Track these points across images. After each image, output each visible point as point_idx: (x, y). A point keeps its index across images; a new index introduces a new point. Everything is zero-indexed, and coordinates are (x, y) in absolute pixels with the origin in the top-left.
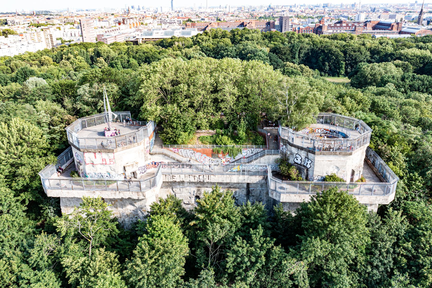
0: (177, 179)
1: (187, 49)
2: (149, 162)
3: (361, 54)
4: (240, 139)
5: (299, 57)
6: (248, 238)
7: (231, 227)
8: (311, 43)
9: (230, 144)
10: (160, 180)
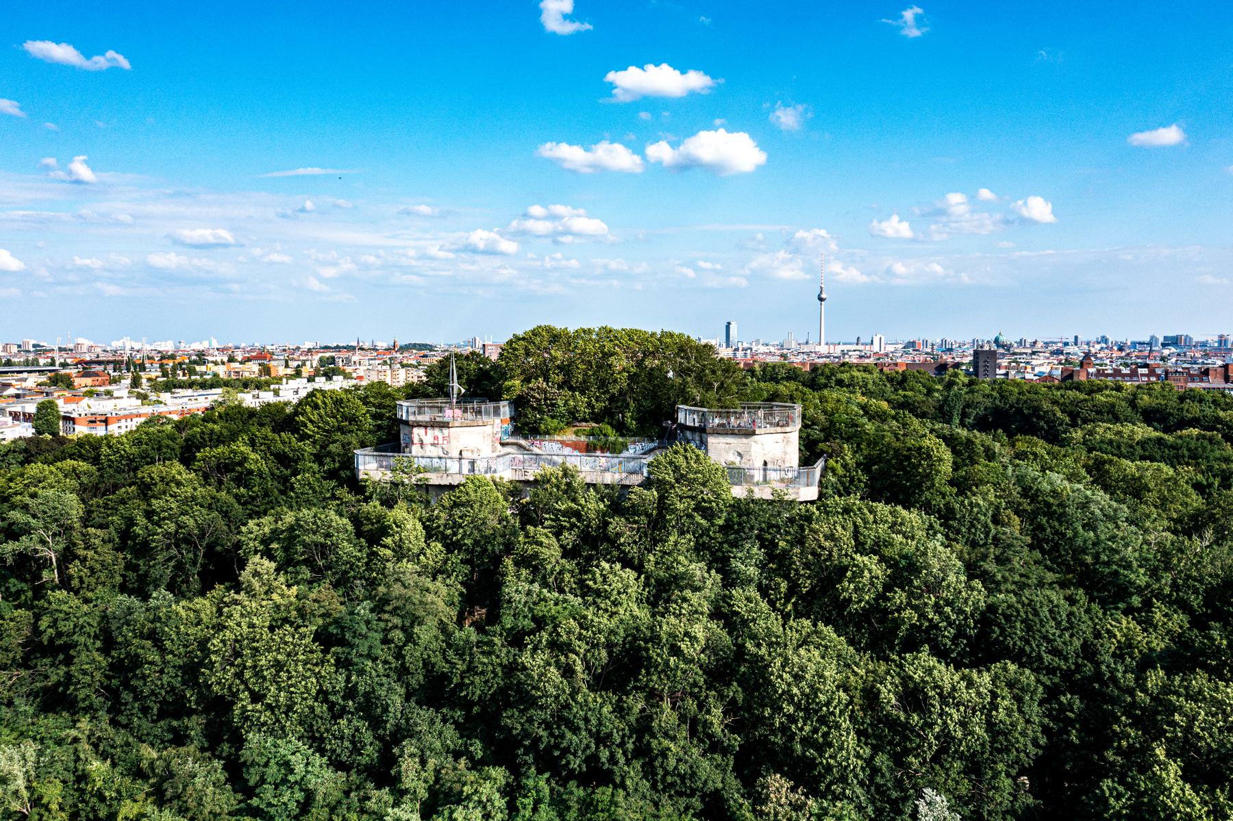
4: (628, 430)
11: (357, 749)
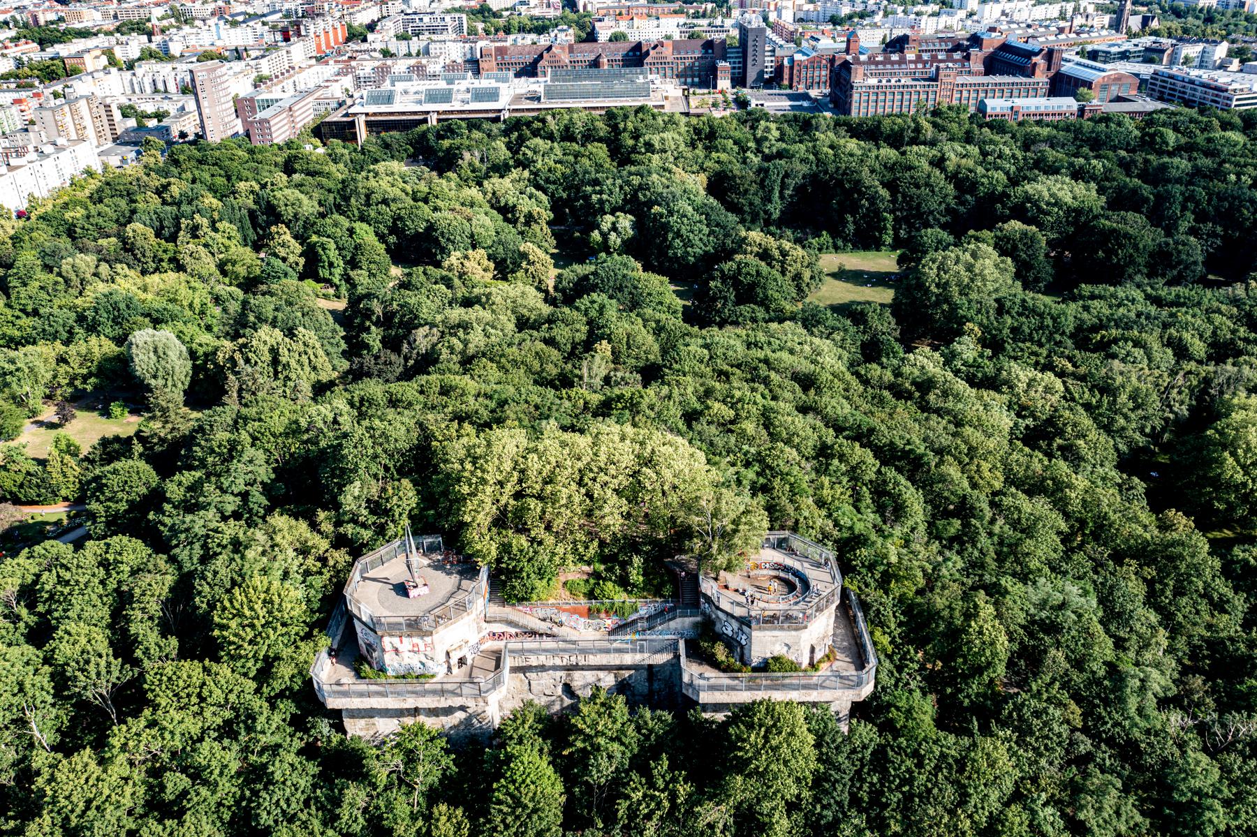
0: (534, 661)
1: (495, 180)
2: (485, 633)
3: (933, 191)
5: (782, 197)
6: (646, 772)
7: (623, 753)
8: (811, 157)
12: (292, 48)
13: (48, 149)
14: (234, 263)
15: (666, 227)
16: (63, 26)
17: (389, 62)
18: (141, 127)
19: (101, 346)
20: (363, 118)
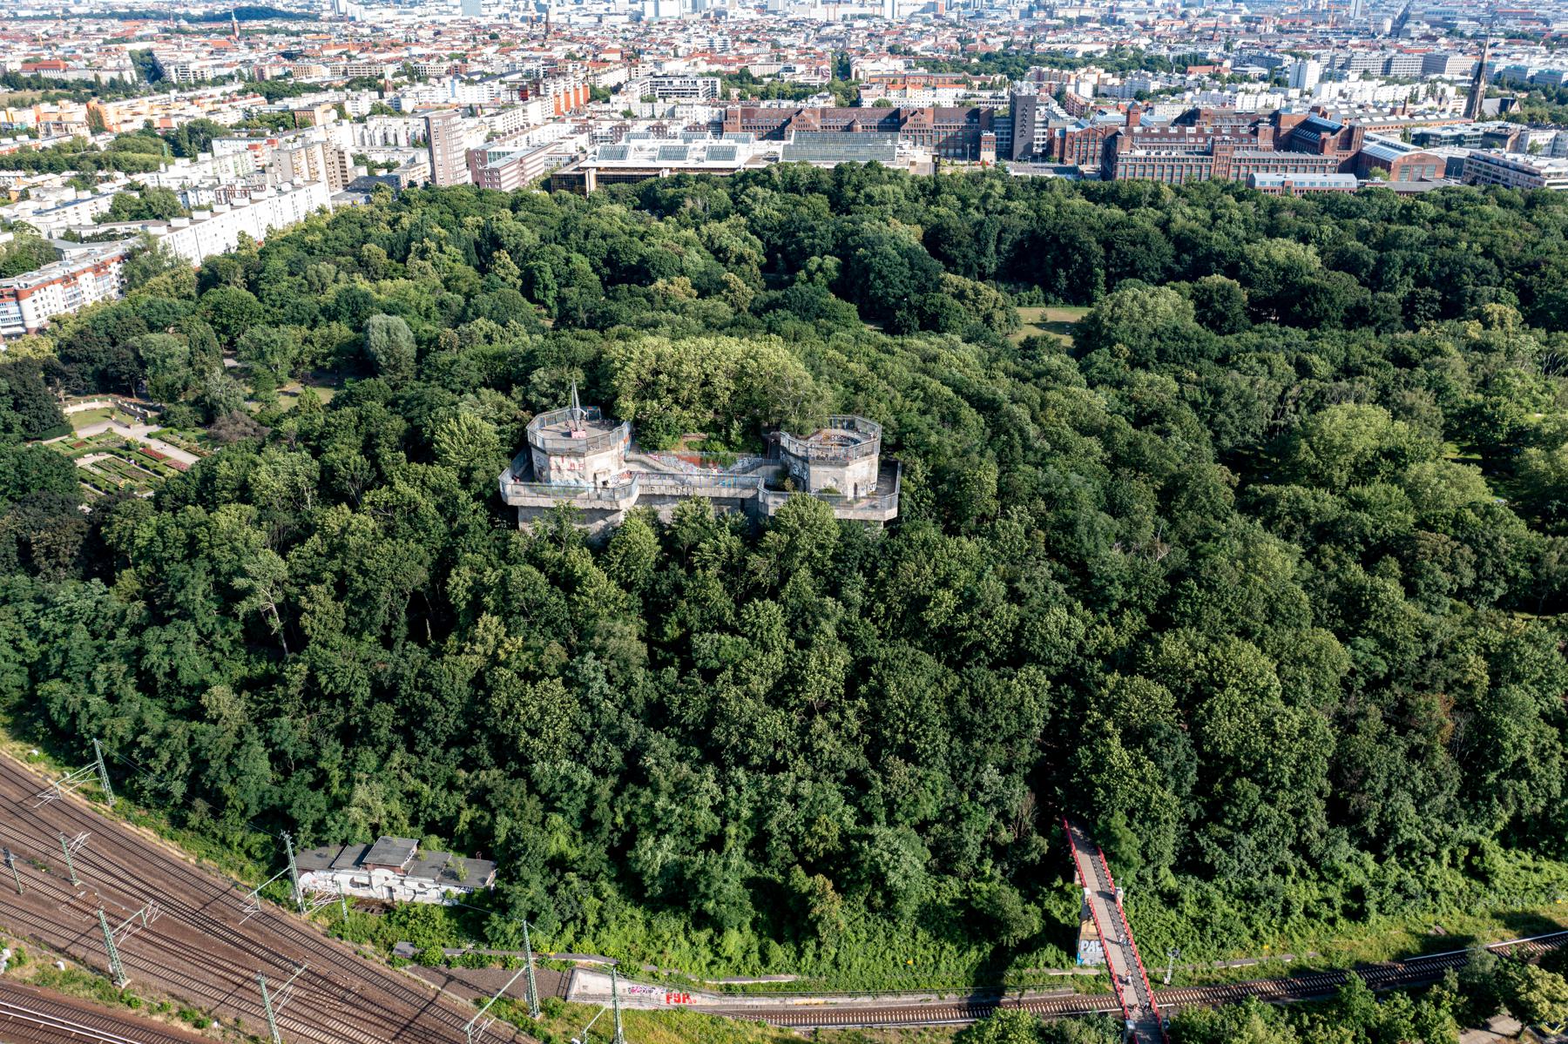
1: (714, 225)
3: (1149, 249)
5: (998, 252)
9: (723, 451)
10: (637, 492)
11: (608, 760)
12: (530, 107)
13: (286, 187)
14: (458, 279)
15: (868, 269)
16: (291, 81)
17: (628, 122)
18: (371, 175)
19: (341, 331)
20: (593, 172)
